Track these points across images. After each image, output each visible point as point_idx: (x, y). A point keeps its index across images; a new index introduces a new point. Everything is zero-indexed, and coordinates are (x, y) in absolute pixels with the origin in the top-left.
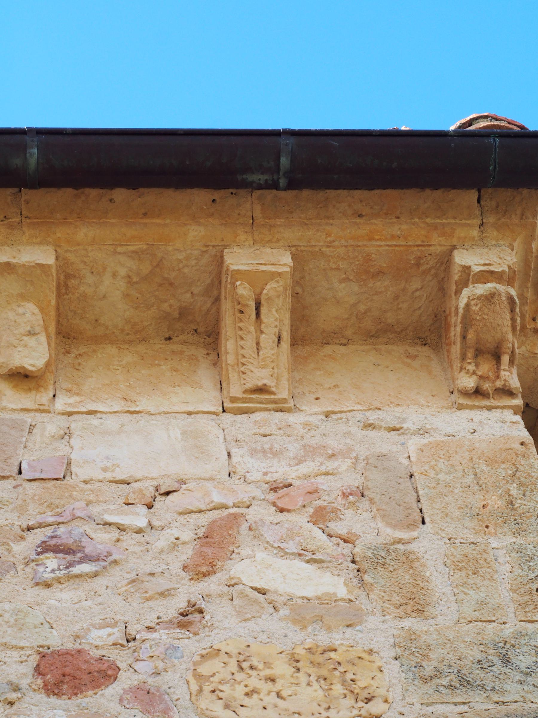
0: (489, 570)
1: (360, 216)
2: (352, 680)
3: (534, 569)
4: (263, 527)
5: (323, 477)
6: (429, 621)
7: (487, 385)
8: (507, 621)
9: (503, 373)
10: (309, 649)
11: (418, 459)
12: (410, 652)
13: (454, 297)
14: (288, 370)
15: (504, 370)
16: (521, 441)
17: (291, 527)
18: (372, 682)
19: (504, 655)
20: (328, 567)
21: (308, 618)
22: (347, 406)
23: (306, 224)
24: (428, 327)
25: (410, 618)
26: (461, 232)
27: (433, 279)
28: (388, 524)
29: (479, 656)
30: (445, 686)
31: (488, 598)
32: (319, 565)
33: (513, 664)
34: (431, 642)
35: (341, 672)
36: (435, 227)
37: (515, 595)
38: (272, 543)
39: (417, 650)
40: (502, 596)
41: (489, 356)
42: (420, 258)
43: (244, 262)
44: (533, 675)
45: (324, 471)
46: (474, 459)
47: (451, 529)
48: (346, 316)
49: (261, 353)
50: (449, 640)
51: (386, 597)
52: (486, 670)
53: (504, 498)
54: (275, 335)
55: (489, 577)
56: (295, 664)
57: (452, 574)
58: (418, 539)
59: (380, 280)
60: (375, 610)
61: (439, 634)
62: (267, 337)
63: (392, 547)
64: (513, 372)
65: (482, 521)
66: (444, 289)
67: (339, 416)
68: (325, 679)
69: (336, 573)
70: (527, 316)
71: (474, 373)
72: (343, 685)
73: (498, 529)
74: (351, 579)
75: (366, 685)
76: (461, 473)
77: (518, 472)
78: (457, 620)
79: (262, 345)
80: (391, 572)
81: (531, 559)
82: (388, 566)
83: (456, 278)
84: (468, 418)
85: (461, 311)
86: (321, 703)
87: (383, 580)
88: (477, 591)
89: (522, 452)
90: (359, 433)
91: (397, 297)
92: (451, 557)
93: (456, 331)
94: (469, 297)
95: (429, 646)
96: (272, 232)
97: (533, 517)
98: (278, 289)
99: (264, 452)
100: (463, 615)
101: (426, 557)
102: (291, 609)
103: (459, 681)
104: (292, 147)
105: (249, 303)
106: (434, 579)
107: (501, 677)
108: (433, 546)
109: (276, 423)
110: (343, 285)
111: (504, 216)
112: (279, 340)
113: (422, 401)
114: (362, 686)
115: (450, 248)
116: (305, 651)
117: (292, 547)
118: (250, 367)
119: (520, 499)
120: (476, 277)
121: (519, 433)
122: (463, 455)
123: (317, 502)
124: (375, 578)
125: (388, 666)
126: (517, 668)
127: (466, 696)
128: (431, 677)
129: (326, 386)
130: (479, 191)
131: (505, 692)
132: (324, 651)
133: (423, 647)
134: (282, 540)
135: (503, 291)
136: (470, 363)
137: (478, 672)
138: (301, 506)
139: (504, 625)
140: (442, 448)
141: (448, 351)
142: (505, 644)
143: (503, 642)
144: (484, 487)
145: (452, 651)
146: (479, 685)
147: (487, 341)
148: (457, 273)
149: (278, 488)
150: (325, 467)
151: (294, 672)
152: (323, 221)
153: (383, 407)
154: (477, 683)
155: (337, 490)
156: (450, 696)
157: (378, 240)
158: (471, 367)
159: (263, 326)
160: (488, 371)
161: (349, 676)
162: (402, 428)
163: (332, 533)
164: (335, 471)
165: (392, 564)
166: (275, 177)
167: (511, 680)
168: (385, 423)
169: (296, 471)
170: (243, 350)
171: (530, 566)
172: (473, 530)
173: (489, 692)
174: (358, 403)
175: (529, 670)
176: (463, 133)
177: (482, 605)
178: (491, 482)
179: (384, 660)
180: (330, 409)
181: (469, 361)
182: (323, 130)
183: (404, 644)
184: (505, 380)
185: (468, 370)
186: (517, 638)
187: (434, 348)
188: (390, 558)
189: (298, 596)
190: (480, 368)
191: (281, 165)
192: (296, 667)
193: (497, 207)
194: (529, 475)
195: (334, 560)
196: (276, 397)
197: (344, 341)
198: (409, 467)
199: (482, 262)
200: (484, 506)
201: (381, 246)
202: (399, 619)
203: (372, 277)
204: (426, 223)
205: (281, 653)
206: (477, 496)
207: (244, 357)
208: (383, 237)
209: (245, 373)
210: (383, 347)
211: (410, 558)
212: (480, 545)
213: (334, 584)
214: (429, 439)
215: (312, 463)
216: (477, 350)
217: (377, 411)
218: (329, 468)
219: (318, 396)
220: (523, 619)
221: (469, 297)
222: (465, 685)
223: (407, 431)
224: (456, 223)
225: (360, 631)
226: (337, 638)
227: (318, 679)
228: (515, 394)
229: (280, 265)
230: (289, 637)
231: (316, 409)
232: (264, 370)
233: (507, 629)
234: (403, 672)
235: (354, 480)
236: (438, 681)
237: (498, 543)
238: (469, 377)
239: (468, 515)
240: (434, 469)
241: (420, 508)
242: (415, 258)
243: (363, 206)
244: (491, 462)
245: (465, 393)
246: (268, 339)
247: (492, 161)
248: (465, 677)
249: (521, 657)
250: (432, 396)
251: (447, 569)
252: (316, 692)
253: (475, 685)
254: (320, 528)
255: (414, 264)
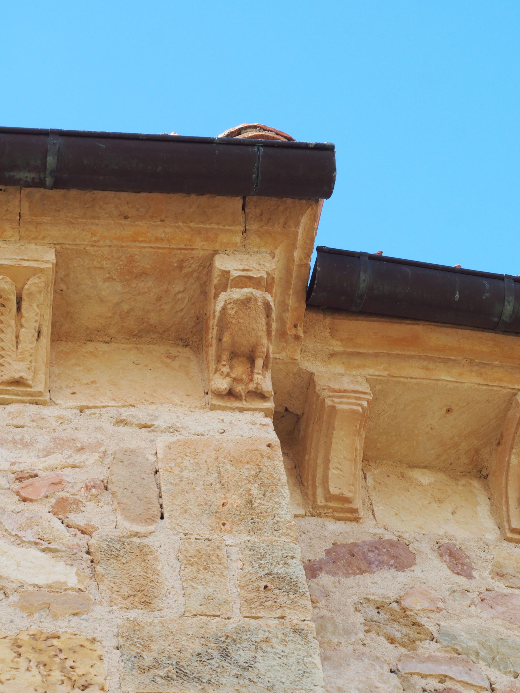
0: (220, 567)
1: (126, 217)
2: (71, 667)
3: (264, 567)
4: (3, 515)
5: (70, 469)
6: (154, 613)
7: (240, 388)
8: (232, 616)
9: (256, 376)
10: (33, 635)
11: (165, 456)
12: (132, 642)
13: (213, 300)
14: (46, 364)
15: (258, 373)
16: (268, 443)
17: (31, 516)
18: (91, 670)
19: (225, 649)
20: (62, 557)
21: (36, 605)
22: (102, 402)
23: (72, 223)
24: (190, 329)
25: (136, 609)
26: (224, 238)
27: (195, 282)
28: (127, 518)
29: (199, 649)
30: (162, 677)
31: (215, 593)
32: (54, 555)
33: (232, 658)
34: (154, 634)
35: (61, 659)
36: (199, 232)
37: (243, 591)
38: (10, 530)
39: (139, 640)
40: (230, 591)
41: (244, 359)
42: (183, 261)
43: (8, 256)
44: (250, 669)
45: (71, 463)
46: (219, 458)
47: (188, 525)
48: (110, 315)
49: (20, 346)
50: (172, 633)
51: (115, 588)
52: (205, 663)
53: (244, 497)
54: (35, 329)
55: (219, 573)
56: (17, 649)
57: (184, 569)
58: (154, 534)
59: (143, 281)
60: (103, 600)
61: (163, 626)
62: (27, 331)
63: (128, 540)
64: (267, 376)
65: (220, 518)
66: (206, 293)
67: (93, 411)
68: (45, 665)
69: (70, 563)
70: (288, 322)
71: (228, 375)
72: (61, 672)
73: (234, 527)
74: (83, 569)
75: (84, 672)
76: (205, 471)
77: (261, 473)
78: (183, 613)
79: (21, 338)
80: (124, 564)
81: (263, 557)
82: (121, 558)
83: (215, 281)
84: (218, 419)
85: (217, 314)
86: (38, 688)
87: (115, 571)
88: (205, 586)
89: (267, 453)
90: (109, 427)
91: (159, 298)
92: (184, 552)
93: (213, 334)
94: (226, 300)
95: (151, 637)
96: (38, 229)
97: (270, 517)
98: (40, 285)
99: (15, 442)
100: (188, 608)
101: (160, 551)
102: (21, 596)
103: (177, 672)
104: (59, 148)
105: (10, 297)
106: (165, 573)
107: (218, 670)
108: (168, 540)
109: (30, 415)
110: (107, 284)
111: (267, 224)
112: (38, 335)
113: (177, 400)
114: (81, 673)
115: (212, 252)
116: (28, 637)
117: (29, 536)
118: (9, 359)
119: (259, 499)
120: (235, 282)
121: (267, 435)
122: (209, 454)
123: (60, 493)
124: (107, 570)
125: (109, 655)
126: (236, 662)
127: (181, 687)
128: (149, 667)
129: (84, 381)
130: (244, 199)
131: (221, 685)
132: (48, 638)
133: (145, 638)
134: (21, 528)
135: (260, 297)
136: (225, 365)
137: (196, 664)
138: (44, 497)
139: (228, 620)
140: (190, 446)
141: (207, 353)
142: (226, 639)
143: (225, 637)
144: (226, 486)
145: (173, 643)
146: (195, 678)
147: (242, 345)
148: (216, 277)
149: (23, 478)
150: (72, 460)
151: (15, 657)
152: (88, 220)
153: (137, 404)
154: (194, 675)
155: (81, 482)
156: (166, 687)
157: (142, 241)
158: (226, 369)
159: (23, 320)
160: (242, 374)
161: (69, 663)
162: (153, 425)
163: (71, 524)
164: (82, 464)
165: (125, 556)
166: (42, 176)
167: (228, 674)
168: (137, 420)
169: (44, 462)
170: (3, 343)
171: (261, 564)
172: (209, 527)
173: (205, 684)
174: (113, 399)
175: (247, 665)
176: (229, 142)
177: (209, 600)
178: (233, 481)
179: (106, 649)
180: (84, 404)
181: (224, 363)
182: (91, 132)
183: (127, 634)
184: (258, 383)
185: (222, 372)
186: (239, 633)
187: (195, 349)
188: (124, 550)
189: (30, 583)
190: (234, 370)
191: (47, 164)
192: (18, 652)
193: (261, 215)
194: (272, 476)
195: (69, 550)
196: (32, 390)
197: (108, 339)
198: (156, 464)
199: (241, 267)
200: (223, 504)
201: (144, 247)
202: (126, 610)
203: (135, 278)
204: (190, 227)
205: (5, 638)
206: (218, 494)
207: (4, 349)
208: (147, 239)
209: (4, 365)
210: (145, 347)
211: (143, 551)
212: (214, 542)
213: (65, 574)
214: (178, 437)
215: (60, 455)
216: (232, 353)
217: (131, 407)
218: (76, 461)
219: (74, 391)
220: (247, 615)
221: (226, 300)
222: (182, 676)
223: (158, 429)
224: (219, 229)
225: (85, 620)
226: (63, 626)
227: (38, 664)
228: (267, 397)
229: (43, 261)
230: (15, 623)
231: (71, 404)
232: (21, 363)
233: (231, 624)
234: (122, 661)
235: (99, 474)
236: (156, 671)
237: (232, 541)
238: (223, 379)
239: (207, 512)
240: (179, 466)
241: (161, 503)
242: (178, 261)
243: (129, 208)
244: (236, 461)
245: (218, 395)
246: (27, 334)
247: (255, 170)
248: (183, 669)
249: (241, 652)
250: (187, 395)
251: (179, 564)
252: (35, 677)
253: (191, 677)
254: (59, 519)
255: (176, 266)
